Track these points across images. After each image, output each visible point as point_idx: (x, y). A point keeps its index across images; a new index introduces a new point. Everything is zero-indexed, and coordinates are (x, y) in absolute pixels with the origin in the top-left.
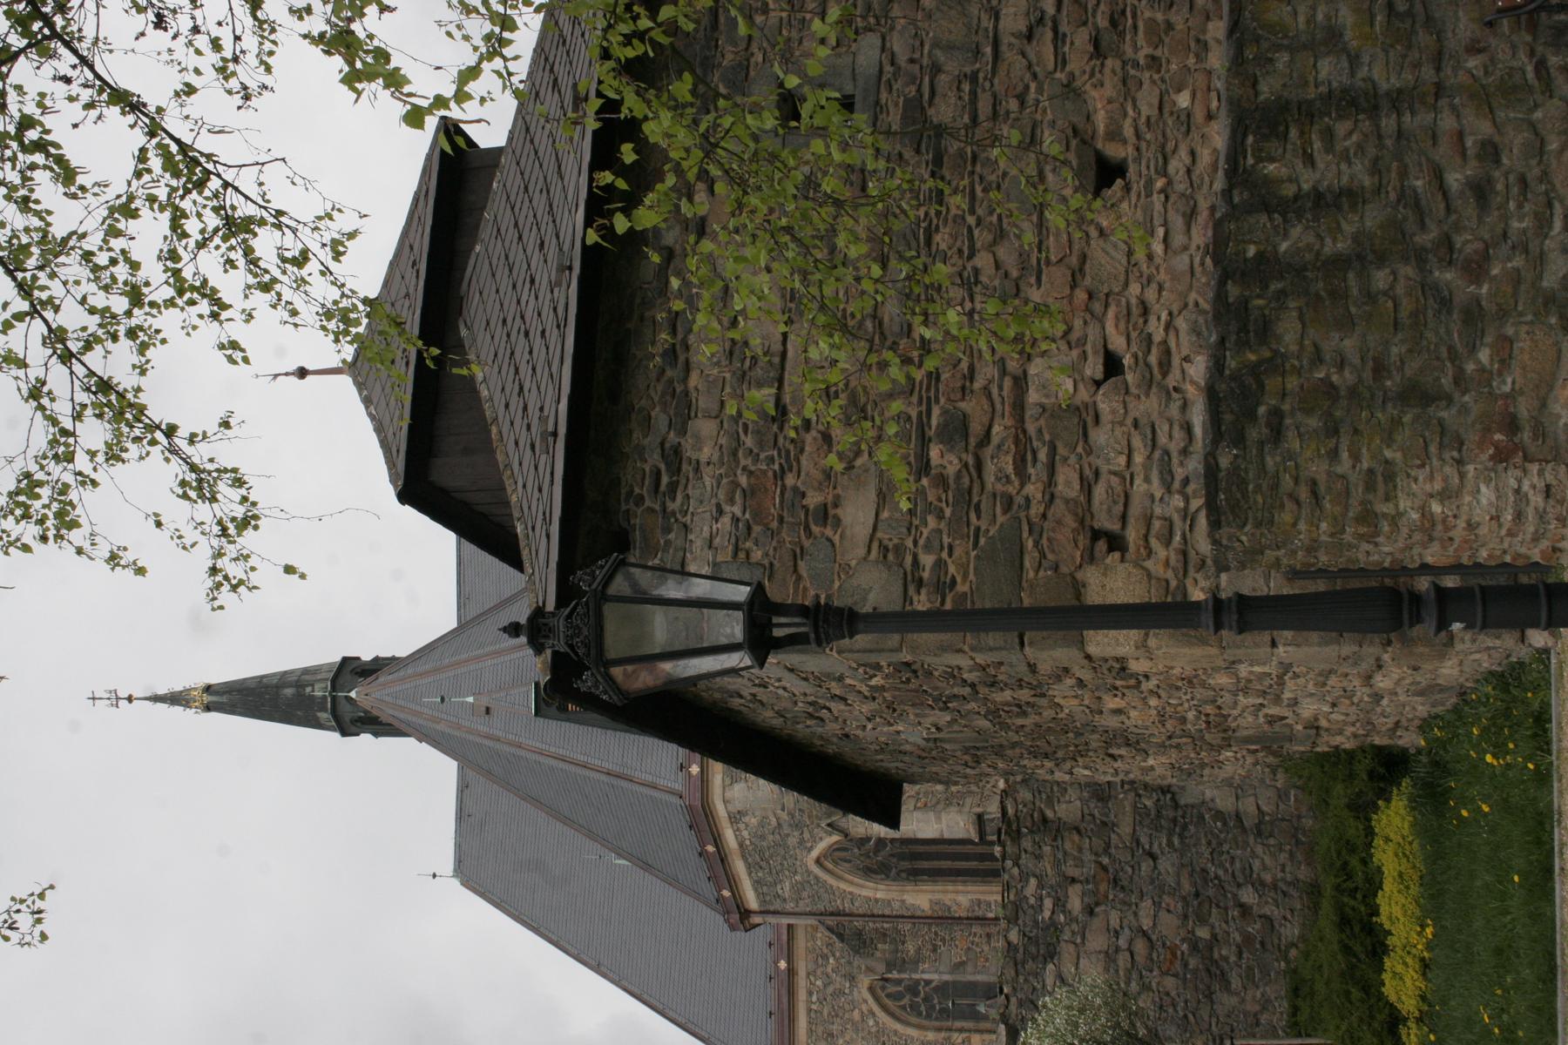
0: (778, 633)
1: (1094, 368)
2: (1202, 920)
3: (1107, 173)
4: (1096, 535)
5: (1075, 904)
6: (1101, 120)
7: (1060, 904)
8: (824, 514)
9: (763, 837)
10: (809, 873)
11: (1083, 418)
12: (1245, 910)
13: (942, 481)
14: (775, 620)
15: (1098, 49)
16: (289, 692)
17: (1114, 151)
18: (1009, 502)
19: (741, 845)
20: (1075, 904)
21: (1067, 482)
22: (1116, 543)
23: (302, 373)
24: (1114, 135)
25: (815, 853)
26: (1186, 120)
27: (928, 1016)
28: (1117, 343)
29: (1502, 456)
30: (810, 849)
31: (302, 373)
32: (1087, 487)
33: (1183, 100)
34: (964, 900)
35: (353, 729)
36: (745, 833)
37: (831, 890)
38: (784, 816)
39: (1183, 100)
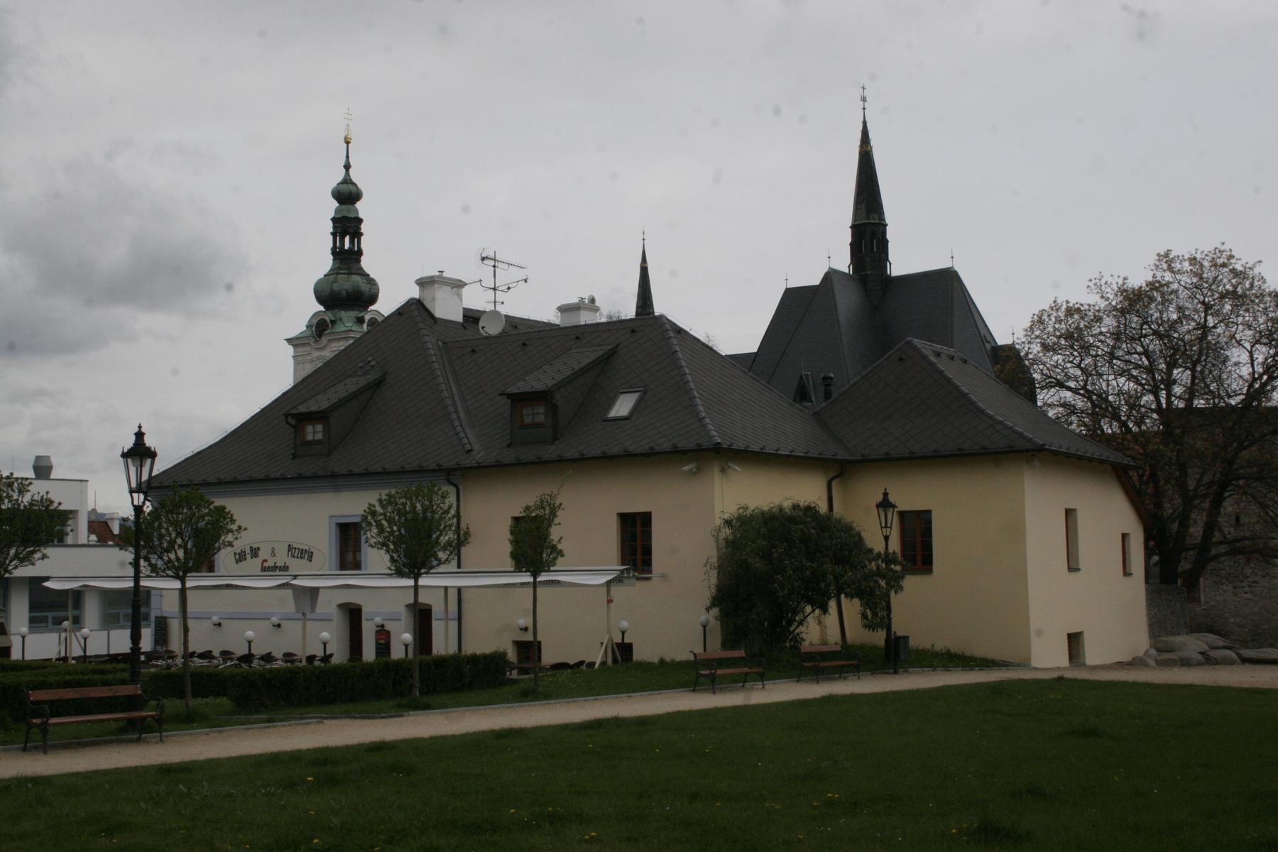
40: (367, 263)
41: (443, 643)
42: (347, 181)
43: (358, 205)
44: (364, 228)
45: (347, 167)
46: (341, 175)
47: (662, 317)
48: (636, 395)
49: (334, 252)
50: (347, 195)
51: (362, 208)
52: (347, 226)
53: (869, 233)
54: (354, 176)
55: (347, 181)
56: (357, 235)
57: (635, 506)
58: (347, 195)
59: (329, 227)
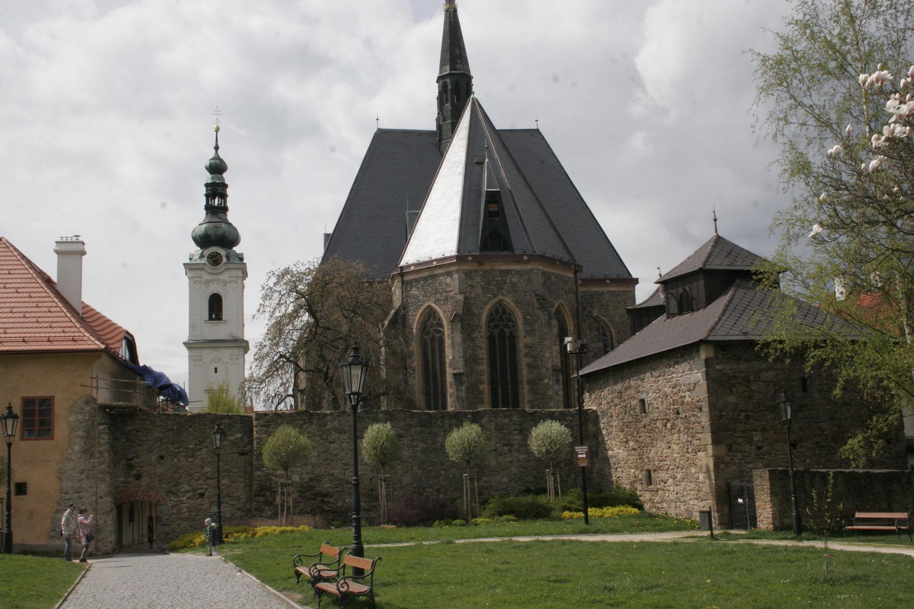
1: (760, 444)
2: (566, 465)
4: (730, 446)
6: (804, 444)
8: (731, 391)
10: (424, 302)
11: (750, 442)
12: (569, 475)
13: (739, 415)
15: (817, 443)
17: (798, 447)
18: (735, 429)
19: (436, 275)
21: (740, 440)
22: (730, 450)
23: (715, 220)
24: (801, 447)
25: (434, 305)
26: (804, 461)
27: (489, 327)
28: (764, 449)
29: (780, 512)
32: (740, 444)
33: (808, 460)
34: (415, 364)
35: (441, 82)
37: (416, 309)
38: (452, 294)
39: (808, 460)
40: (231, 217)
42: (217, 157)
43: (224, 175)
44: (229, 191)
45: (217, 148)
46: (212, 154)
50: (217, 168)
51: (227, 177)
52: (216, 191)
54: (221, 153)
55: (217, 157)
56: (224, 196)
58: (217, 168)
59: (203, 190)
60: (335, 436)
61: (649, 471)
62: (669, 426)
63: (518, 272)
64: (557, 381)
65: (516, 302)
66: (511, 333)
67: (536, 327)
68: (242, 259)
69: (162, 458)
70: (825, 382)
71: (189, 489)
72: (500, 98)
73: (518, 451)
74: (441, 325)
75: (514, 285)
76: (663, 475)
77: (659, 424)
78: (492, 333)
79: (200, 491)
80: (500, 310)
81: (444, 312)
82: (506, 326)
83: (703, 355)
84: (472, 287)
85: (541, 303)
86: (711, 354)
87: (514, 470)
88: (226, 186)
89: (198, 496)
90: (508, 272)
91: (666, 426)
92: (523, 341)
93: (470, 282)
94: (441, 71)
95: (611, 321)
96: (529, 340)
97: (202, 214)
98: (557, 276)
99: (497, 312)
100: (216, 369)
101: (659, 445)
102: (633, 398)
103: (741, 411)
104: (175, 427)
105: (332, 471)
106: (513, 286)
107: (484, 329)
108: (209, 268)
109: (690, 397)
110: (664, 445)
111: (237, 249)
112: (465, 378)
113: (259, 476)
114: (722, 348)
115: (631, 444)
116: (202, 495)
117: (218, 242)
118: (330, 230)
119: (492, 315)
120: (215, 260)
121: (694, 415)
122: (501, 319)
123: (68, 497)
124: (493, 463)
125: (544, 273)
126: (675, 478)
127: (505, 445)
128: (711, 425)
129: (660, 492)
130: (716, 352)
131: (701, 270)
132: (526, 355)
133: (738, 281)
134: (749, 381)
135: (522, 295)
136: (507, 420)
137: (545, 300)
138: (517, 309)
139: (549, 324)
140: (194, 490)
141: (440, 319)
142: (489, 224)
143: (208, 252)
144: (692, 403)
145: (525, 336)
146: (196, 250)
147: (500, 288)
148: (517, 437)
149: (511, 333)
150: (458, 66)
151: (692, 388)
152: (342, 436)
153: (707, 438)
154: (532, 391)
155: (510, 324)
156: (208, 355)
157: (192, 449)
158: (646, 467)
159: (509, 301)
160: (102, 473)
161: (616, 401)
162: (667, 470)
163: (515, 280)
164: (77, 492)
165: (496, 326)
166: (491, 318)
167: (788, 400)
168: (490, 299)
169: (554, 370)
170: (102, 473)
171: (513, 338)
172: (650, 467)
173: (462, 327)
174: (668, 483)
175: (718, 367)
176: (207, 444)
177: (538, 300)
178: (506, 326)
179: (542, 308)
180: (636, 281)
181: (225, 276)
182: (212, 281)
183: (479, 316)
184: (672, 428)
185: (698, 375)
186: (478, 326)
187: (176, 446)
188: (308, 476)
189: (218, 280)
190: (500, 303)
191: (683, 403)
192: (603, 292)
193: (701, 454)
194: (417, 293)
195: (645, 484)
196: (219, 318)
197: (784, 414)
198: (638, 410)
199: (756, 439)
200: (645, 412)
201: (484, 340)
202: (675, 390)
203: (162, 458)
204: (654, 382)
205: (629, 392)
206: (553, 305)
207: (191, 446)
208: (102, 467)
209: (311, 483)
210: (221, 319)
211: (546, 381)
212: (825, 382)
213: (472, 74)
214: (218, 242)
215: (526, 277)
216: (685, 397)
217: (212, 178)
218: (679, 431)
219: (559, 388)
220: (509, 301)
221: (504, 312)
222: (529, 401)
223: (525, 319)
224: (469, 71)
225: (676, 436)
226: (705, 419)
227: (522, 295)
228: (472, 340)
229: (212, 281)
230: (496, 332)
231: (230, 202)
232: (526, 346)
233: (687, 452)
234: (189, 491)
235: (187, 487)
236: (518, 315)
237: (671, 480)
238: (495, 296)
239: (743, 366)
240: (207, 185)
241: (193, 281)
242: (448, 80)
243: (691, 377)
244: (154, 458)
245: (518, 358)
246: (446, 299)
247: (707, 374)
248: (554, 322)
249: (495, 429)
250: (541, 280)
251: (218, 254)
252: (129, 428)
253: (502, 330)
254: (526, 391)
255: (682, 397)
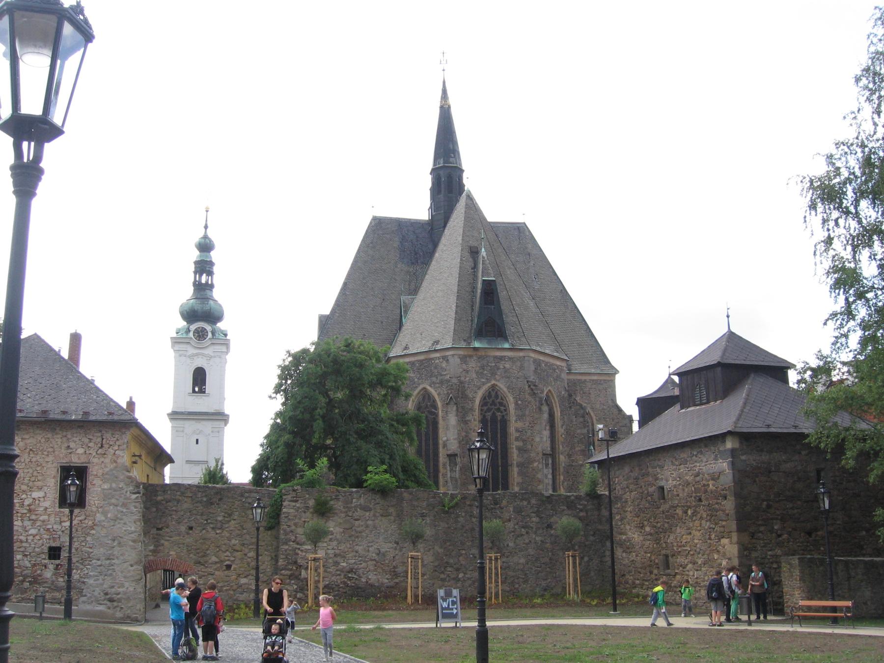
0: (25, 145)
1: (779, 532)
3: (809, 534)
5: (581, 514)
7: (581, 510)
9: (436, 368)
11: (771, 531)
14: (33, 144)
16: (451, 146)
19: (432, 359)
20: (581, 514)
23: (728, 316)
25: (429, 388)
30: (430, 386)
31: (728, 316)
36: (437, 361)
38: (448, 377)
41: (736, 562)
42: (205, 237)
43: (212, 253)
44: (215, 269)
45: (206, 227)
46: (202, 234)
47: (36, 338)
48: (125, 407)
49: (194, 284)
50: (205, 246)
51: (214, 255)
52: (204, 267)
53: (447, 181)
55: (205, 237)
56: (210, 273)
57: (76, 460)
58: (205, 246)
60: (359, 513)
61: (667, 556)
62: (689, 512)
63: (510, 359)
64: (547, 465)
65: (508, 388)
66: (503, 416)
67: (527, 413)
68: (226, 335)
69: (191, 528)
70: (837, 474)
71: (217, 560)
72: (495, 194)
73: (535, 533)
74: (436, 407)
75: (506, 370)
76: (680, 560)
77: (679, 511)
78: (484, 416)
79: (227, 563)
80: (493, 394)
81: (439, 394)
82: (498, 410)
83: (729, 444)
84: (467, 372)
85: (532, 390)
86: (737, 445)
87: (531, 551)
88: (211, 264)
89: (224, 568)
90: (502, 358)
91: (686, 512)
92: (514, 425)
93: (464, 366)
94: (434, 165)
95: (592, 408)
96: (520, 425)
97: (189, 291)
98: (546, 364)
99: (490, 395)
100: (197, 440)
101: (678, 530)
102: (651, 485)
103: (763, 500)
104: (205, 499)
105: (357, 548)
106: (506, 372)
107: (477, 412)
108: (194, 341)
109: (713, 485)
110: (683, 531)
111: (220, 325)
112: (458, 460)
113: (286, 551)
114: (746, 438)
115: (648, 529)
116: (229, 567)
117: (202, 316)
118: (327, 311)
119: (485, 398)
120: (201, 335)
121: (717, 503)
122: (493, 403)
123: (99, 563)
124: (511, 544)
125: (535, 361)
126: (694, 563)
127: (523, 527)
128: (737, 512)
129: (678, 577)
130: (741, 443)
131: (719, 364)
132: (517, 439)
133: (752, 375)
134: (770, 472)
135: (514, 380)
136: (525, 503)
137: (535, 386)
138: (509, 395)
139: (540, 409)
140: (222, 561)
141: (434, 401)
142: (487, 314)
143: (193, 327)
144: (716, 491)
145: (516, 421)
146: (183, 324)
147: (493, 374)
148: (534, 519)
149: (503, 416)
150: (451, 160)
151: (715, 477)
152: (367, 514)
153: (733, 525)
154: (520, 473)
155: (502, 408)
156: (190, 426)
157: (220, 521)
158: (663, 552)
159: (502, 386)
160: (134, 541)
161: (631, 487)
162: (687, 556)
163: (507, 366)
164: (108, 559)
165: (489, 410)
166: (484, 402)
167: (828, 493)
168: (484, 384)
169: (544, 454)
170: (134, 541)
171: (504, 423)
172: (668, 552)
173: (457, 410)
174: (688, 568)
175: (743, 458)
176: (236, 517)
177: (529, 386)
178: (498, 410)
179: (533, 394)
180: (617, 372)
181: (209, 351)
182: (197, 355)
183: (473, 400)
184: (694, 514)
185: (724, 465)
186: (472, 409)
187: (205, 517)
188: (333, 551)
189: (203, 355)
190: (494, 386)
191: (706, 491)
192: (585, 381)
193: (725, 541)
194: (412, 375)
195: (662, 568)
196: (202, 391)
197: (822, 505)
198: (656, 496)
199: (776, 527)
200: (664, 498)
201: (477, 423)
202: (698, 479)
203: (191, 528)
204: (674, 470)
205: (646, 479)
206: (542, 392)
207: (220, 518)
208: (132, 535)
209: (336, 559)
210: (204, 392)
211: (535, 464)
212: (837, 474)
213: (464, 168)
214: (202, 316)
215: (518, 364)
216: (708, 485)
217: (200, 256)
218: (701, 518)
219: (548, 472)
220: (502, 386)
221: (497, 396)
222: (518, 483)
223: (516, 404)
224: (460, 164)
225: (697, 523)
226: (729, 505)
227: (514, 380)
228: (466, 422)
229: (197, 355)
230: (489, 415)
231: (191, 278)
232: (517, 430)
233: (710, 539)
234: (216, 563)
235: (214, 559)
236: (511, 399)
237: (690, 566)
238: (488, 380)
239: (765, 457)
240: (196, 263)
241: (179, 354)
242: (441, 172)
243: (718, 467)
244: (183, 528)
245: (508, 441)
246: (442, 382)
247: (733, 464)
248: (545, 408)
249: (514, 511)
250: (532, 368)
251: (204, 330)
252: (159, 498)
253: (494, 414)
254: (516, 473)
255: (704, 485)
